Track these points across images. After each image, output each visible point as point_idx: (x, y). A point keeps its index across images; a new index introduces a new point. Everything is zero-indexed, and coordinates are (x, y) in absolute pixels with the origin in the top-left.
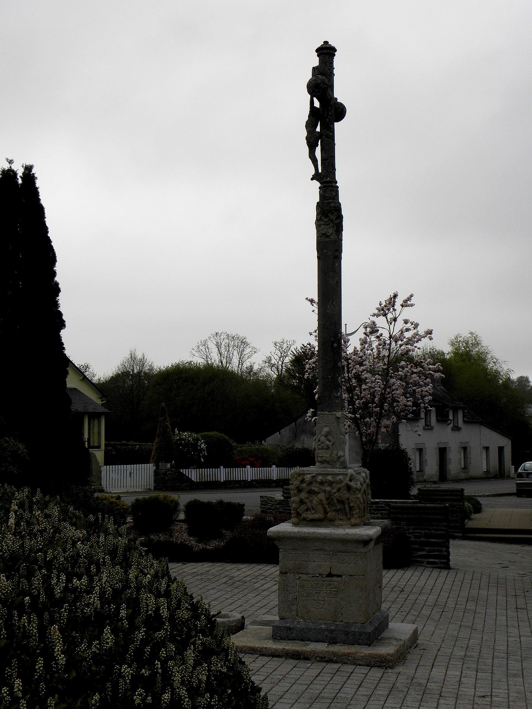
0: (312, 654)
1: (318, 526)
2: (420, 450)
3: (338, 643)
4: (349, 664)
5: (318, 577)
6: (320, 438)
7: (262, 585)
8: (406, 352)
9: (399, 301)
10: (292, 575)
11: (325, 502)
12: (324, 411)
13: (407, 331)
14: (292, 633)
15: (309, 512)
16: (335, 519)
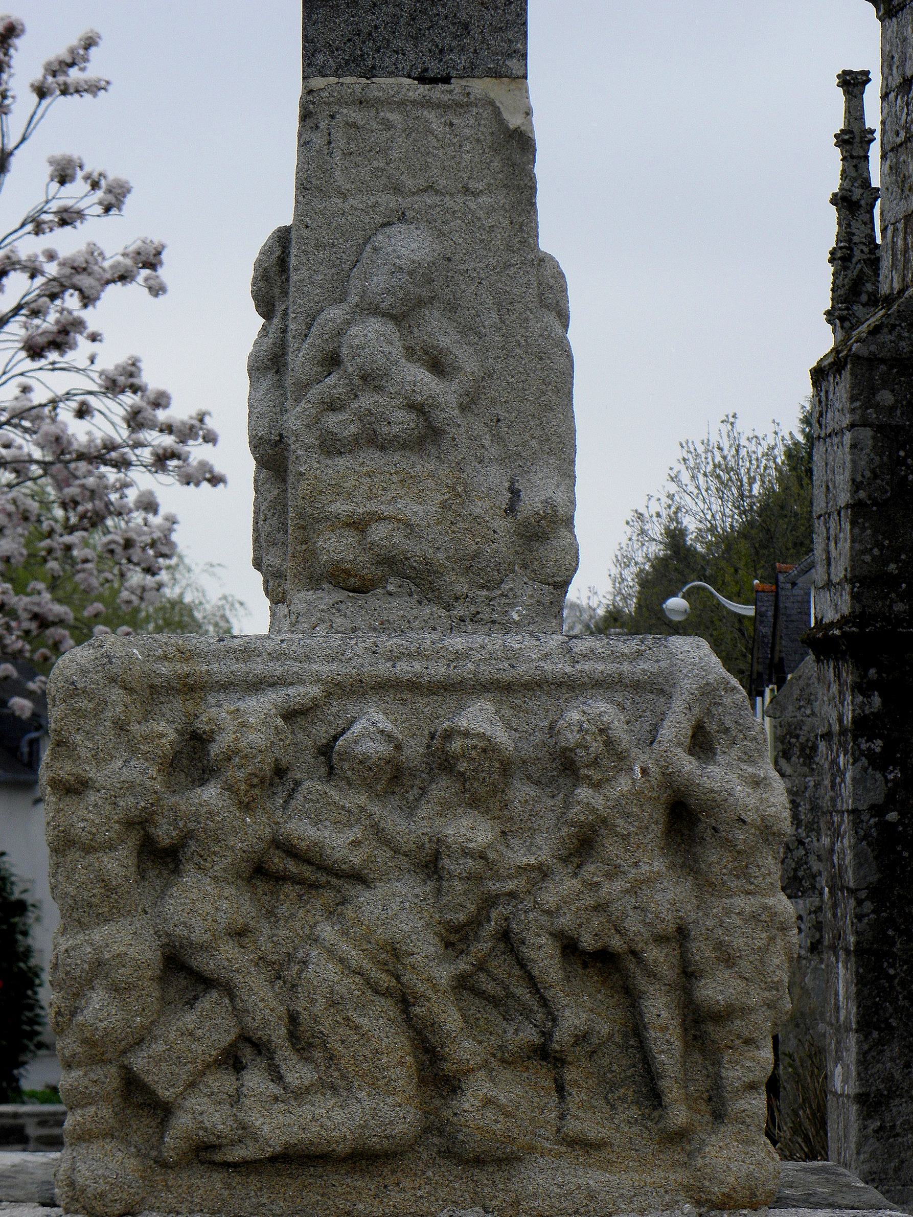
6: (340, 333)
8: (59, 332)
12: (370, 73)
13: (63, 223)
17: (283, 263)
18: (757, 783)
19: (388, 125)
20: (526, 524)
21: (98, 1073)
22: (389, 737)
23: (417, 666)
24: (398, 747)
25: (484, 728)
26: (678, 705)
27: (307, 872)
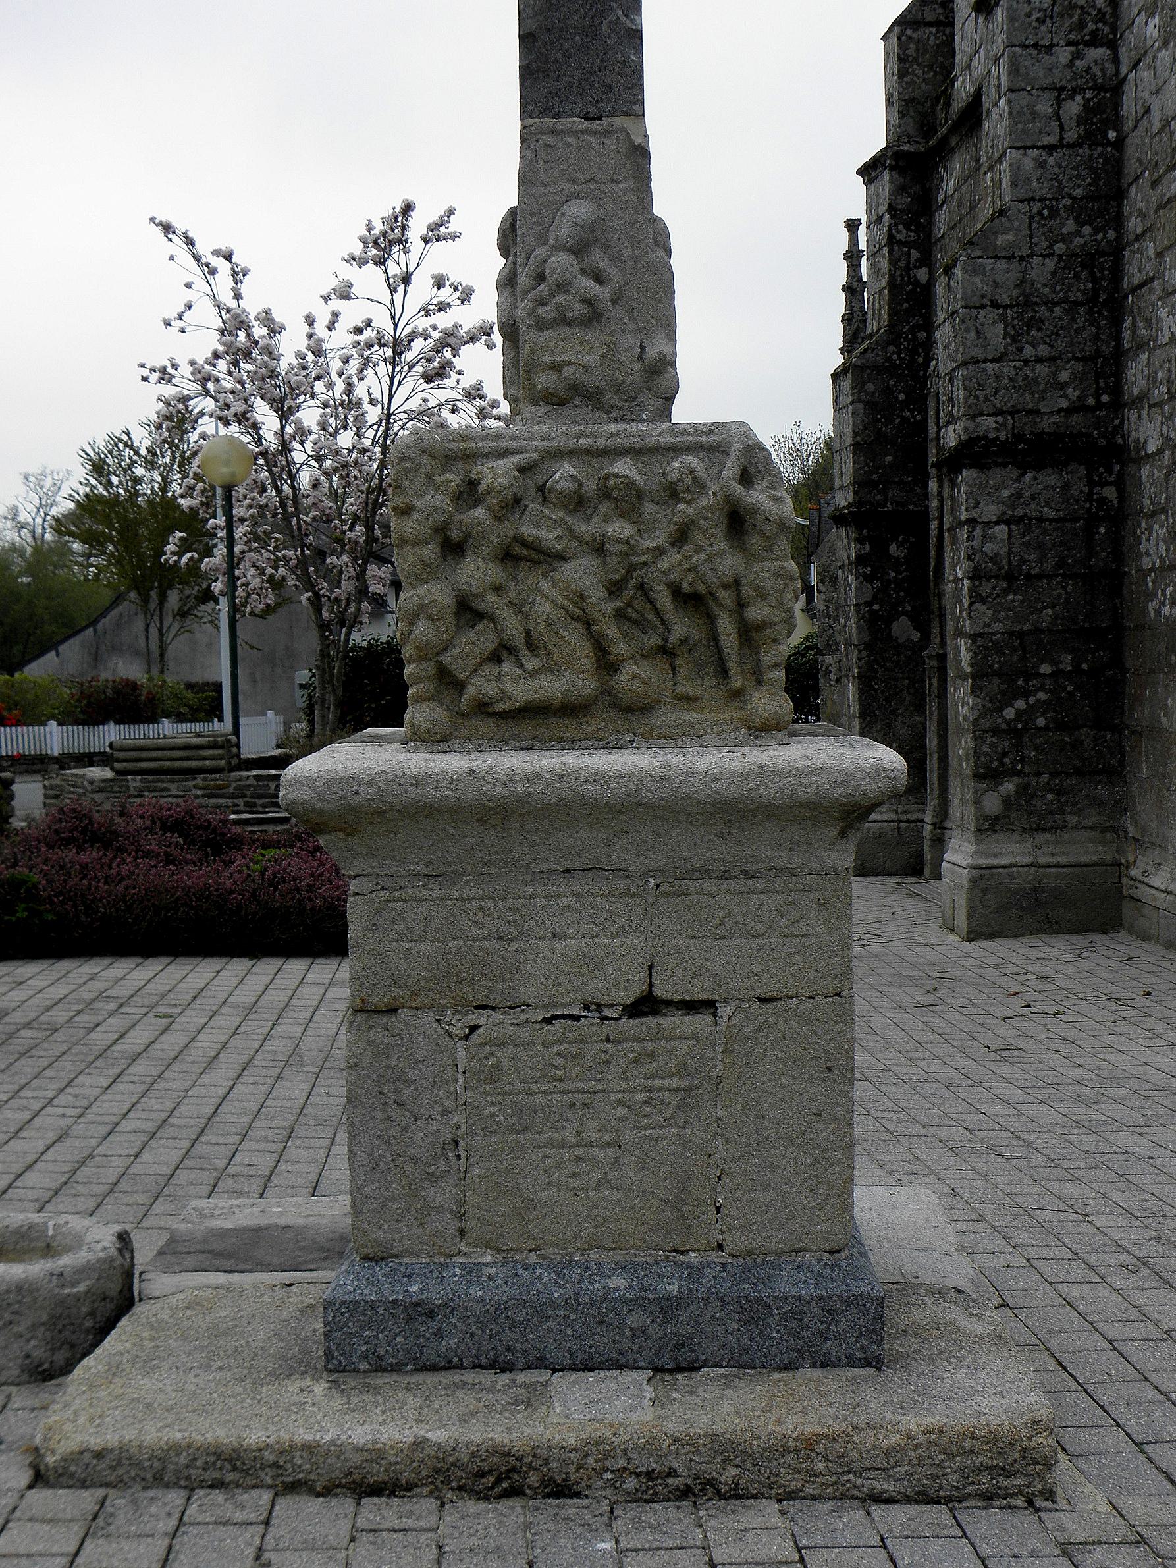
0: (591, 1461)
1: (562, 740)
3: (705, 1365)
4: (814, 1498)
5: (577, 1018)
6: (545, 262)
7: (121, 1037)
9: (417, 226)
10: (429, 1016)
11: (602, 606)
12: (557, 116)
13: (440, 310)
14: (439, 1335)
15: (508, 667)
16: (658, 702)
17: (513, 226)
18: (776, 499)
19: (568, 145)
20: (649, 365)
21: (424, 665)
22: (575, 479)
23: (590, 441)
24: (581, 485)
25: (627, 472)
26: (733, 458)
27: (533, 555)
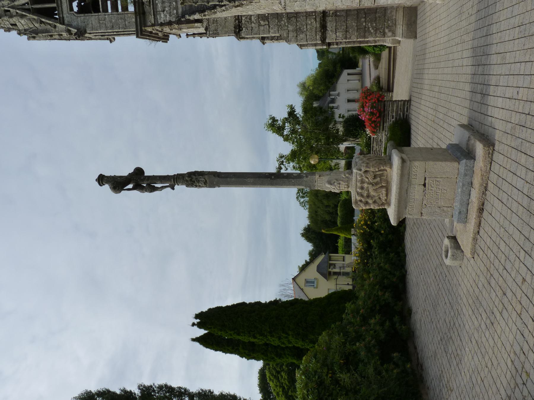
2: (348, 111)
14: (463, 211)
